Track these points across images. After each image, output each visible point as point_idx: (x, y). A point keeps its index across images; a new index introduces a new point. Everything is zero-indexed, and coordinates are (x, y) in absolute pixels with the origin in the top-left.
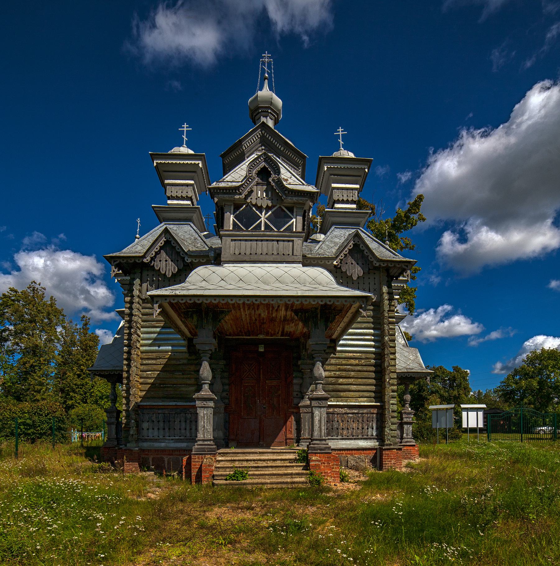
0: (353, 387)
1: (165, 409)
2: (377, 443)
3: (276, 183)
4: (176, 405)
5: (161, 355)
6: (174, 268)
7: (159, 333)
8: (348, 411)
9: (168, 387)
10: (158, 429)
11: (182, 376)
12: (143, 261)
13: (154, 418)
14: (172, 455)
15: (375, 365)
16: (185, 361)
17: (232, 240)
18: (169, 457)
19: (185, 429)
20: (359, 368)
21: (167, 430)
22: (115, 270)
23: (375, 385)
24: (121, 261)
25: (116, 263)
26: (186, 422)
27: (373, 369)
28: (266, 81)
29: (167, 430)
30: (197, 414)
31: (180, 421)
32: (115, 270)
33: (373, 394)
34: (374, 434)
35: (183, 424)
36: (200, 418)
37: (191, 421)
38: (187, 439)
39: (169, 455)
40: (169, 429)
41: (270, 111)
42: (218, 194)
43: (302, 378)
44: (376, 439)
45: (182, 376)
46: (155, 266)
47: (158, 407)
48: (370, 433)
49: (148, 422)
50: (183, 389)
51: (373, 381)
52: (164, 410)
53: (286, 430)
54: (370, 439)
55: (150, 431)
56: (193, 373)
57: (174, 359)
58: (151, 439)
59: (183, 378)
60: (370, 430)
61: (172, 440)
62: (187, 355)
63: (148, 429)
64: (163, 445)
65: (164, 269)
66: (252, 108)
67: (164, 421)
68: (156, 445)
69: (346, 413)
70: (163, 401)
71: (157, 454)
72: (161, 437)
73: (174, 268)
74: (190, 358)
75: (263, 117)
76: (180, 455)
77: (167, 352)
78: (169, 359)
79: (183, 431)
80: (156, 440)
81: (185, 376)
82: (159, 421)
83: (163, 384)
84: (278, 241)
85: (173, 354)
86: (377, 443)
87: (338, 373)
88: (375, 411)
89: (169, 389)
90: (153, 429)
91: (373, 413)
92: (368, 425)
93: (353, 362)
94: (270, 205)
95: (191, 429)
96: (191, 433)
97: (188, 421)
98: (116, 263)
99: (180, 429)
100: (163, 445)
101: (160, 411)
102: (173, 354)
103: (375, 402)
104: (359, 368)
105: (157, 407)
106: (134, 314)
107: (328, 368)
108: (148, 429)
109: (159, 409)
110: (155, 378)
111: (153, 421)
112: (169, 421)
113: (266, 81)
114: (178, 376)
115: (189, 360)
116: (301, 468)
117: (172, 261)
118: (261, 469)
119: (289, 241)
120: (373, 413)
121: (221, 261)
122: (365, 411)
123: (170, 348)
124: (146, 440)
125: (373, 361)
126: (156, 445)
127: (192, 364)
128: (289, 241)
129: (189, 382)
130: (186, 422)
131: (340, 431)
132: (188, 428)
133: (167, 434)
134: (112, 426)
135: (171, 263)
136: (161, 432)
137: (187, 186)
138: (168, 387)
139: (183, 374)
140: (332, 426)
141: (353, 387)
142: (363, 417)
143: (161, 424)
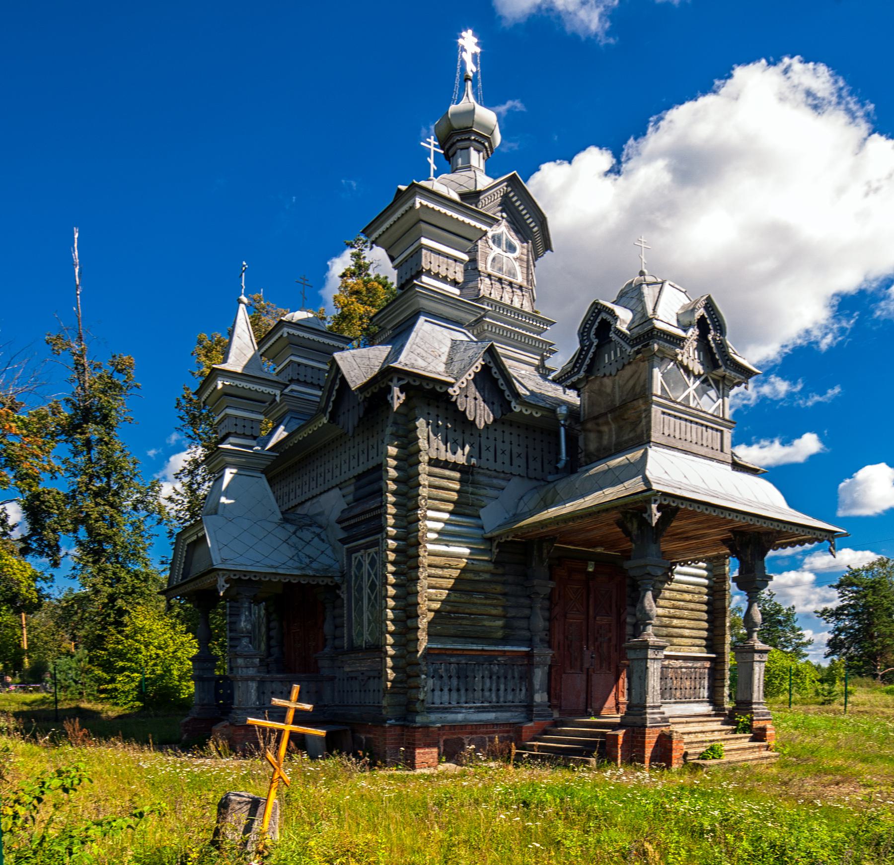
0: (687, 632)
1: (460, 655)
2: (711, 708)
3: (717, 345)
4: (483, 650)
5: (453, 562)
6: (489, 416)
7: (446, 522)
8: (684, 665)
9: (463, 618)
10: (450, 690)
11: (484, 602)
12: (447, 391)
13: (442, 671)
14: (476, 733)
15: (706, 603)
16: (487, 576)
17: (664, 413)
18: (471, 737)
19: (490, 690)
20: (692, 606)
21: (463, 692)
22: (400, 395)
23: (707, 630)
24: (424, 384)
25: (402, 383)
26: (491, 678)
27: (705, 607)
28: (469, 83)
29: (463, 692)
30: (647, 668)
31: (483, 677)
32: (400, 395)
33: (704, 643)
34: (706, 694)
35: (488, 681)
36: (650, 674)
37: (498, 677)
38: (492, 707)
39: (471, 733)
40: (467, 690)
41: (487, 144)
42: (660, 338)
43: (531, 608)
44: (708, 702)
45: (484, 602)
46: (458, 404)
47: (452, 653)
48: (701, 695)
49: (433, 677)
50: (486, 623)
51: (706, 625)
52: (460, 658)
53: (617, 690)
54: (702, 702)
55: (437, 693)
56: (500, 597)
57: (471, 571)
58: (438, 708)
59: (485, 605)
60: (702, 689)
61: (471, 708)
62: (491, 567)
63: (433, 690)
64: (460, 717)
65: (473, 413)
66: (456, 124)
67: (458, 677)
68: (450, 717)
69: (681, 668)
70: (454, 642)
71: (453, 734)
72: (454, 704)
73: (489, 416)
74: (495, 571)
75: (475, 149)
76: (487, 733)
77: (459, 557)
78: (463, 570)
79: (487, 694)
80: (445, 710)
81: (488, 602)
82: (450, 677)
83: (454, 613)
84: (707, 427)
85: (470, 562)
86: (711, 708)
87: (672, 611)
88: (708, 664)
89: (464, 622)
90: (442, 690)
91: (705, 668)
92: (700, 683)
93: (688, 597)
94: (702, 372)
95: (498, 690)
96: (498, 696)
97: (494, 677)
98: (402, 383)
99: (483, 690)
100: (460, 717)
101: (453, 660)
102: (470, 562)
103: (708, 653)
104: (692, 606)
105: (450, 652)
106: (422, 483)
107: (662, 602)
108: (433, 690)
109: (452, 656)
110: (443, 601)
111: (442, 677)
112: (467, 677)
113: (469, 83)
114: (478, 601)
115: (493, 574)
116: (748, 740)
117: (484, 401)
118: (697, 745)
119: (717, 430)
120: (705, 668)
121: (650, 442)
122: (699, 664)
123: (467, 551)
124: (430, 710)
125: (706, 598)
126: (450, 717)
127: (496, 582)
128: (717, 430)
129: (494, 612)
130: (491, 678)
131: (673, 691)
132: (494, 688)
133: (463, 699)
134: (250, 683)
135: (482, 404)
136: (454, 695)
137: (439, 254)
138: (463, 618)
139: (486, 598)
140: (666, 684)
141: (687, 632)
142: (696, 672)
143: (455, 682)
